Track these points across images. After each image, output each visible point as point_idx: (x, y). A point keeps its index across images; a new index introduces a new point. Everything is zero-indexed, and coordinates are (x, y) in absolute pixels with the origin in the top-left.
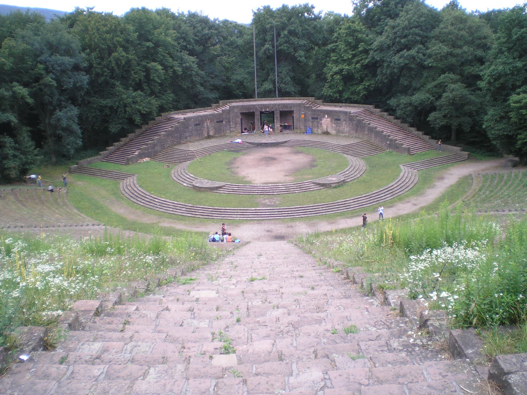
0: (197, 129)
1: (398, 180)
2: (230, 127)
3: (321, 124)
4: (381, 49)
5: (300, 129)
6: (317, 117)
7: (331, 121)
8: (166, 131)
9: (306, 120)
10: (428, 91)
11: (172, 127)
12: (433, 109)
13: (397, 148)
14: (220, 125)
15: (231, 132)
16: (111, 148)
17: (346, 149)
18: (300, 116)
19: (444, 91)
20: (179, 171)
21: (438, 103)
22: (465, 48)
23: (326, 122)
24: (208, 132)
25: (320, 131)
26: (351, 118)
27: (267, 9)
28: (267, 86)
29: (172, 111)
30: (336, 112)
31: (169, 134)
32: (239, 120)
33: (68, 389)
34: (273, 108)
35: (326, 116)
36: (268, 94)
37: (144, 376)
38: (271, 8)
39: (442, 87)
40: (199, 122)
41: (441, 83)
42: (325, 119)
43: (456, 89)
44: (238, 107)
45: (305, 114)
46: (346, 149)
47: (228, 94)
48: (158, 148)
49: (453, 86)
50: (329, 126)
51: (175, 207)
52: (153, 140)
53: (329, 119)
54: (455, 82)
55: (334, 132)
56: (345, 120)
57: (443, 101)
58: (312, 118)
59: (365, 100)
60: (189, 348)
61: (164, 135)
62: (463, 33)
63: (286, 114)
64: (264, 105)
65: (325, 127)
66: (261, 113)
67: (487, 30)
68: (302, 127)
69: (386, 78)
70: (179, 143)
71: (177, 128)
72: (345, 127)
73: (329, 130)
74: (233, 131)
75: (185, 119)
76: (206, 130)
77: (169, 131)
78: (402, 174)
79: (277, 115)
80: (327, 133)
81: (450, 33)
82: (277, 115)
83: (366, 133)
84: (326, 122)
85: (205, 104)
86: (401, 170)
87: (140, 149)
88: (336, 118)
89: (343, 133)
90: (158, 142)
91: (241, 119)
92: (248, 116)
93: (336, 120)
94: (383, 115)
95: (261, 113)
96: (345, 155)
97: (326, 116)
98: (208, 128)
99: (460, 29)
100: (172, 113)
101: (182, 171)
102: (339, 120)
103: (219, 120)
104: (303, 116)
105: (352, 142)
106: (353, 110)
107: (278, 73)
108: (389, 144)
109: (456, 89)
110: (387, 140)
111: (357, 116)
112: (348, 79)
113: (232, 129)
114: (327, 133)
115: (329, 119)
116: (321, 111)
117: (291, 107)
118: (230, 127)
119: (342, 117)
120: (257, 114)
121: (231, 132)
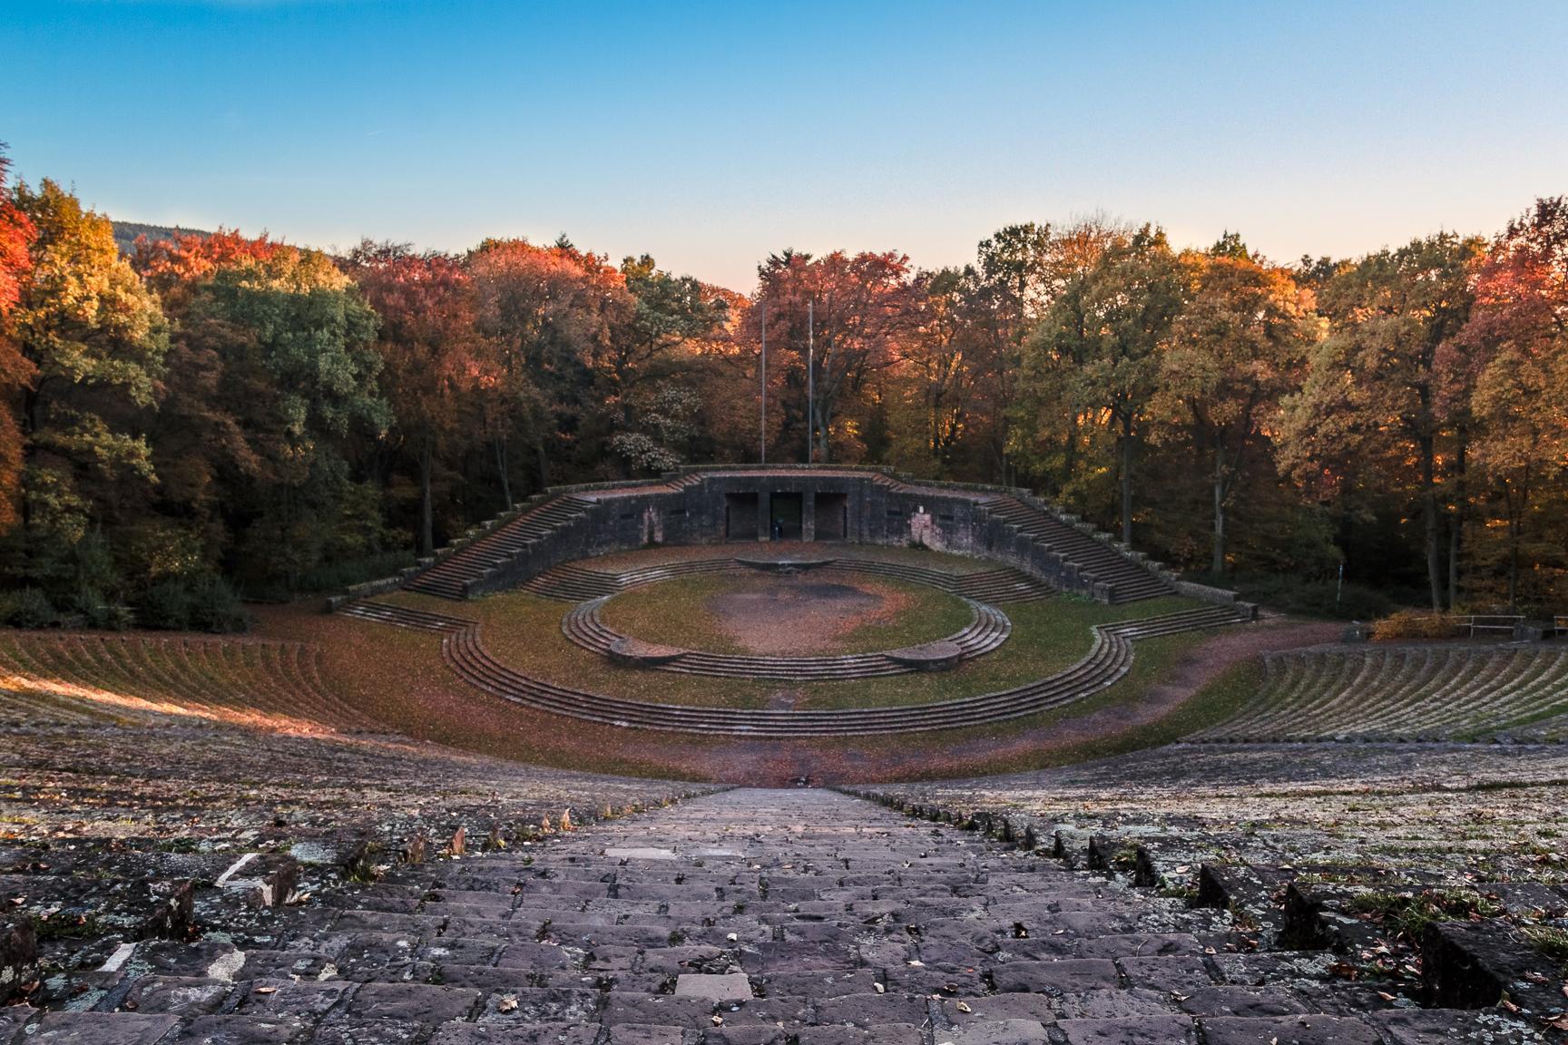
1: (1087, 658)
7: (933, 522)
8: (555, 528)
24: (651, 534)
26: (974, 517)
27: (794, 262)
30: (945, 500)
33: (1190, 971)
37: (221, 1004)
38: (952, 270)
51: (1342, 702)
53: (927, 517)
58: (890, 513)
60: (606, 959)
66: (774, 496)
67: (1299, 303)
71: (579, 521)
73: (926, 541)
78: (1095, 647)
79: (810, 503)
82: (810, 503)
86: (1093, 639)
88: (945, 517)
95: (774, 496)
98: (651, 527)
101: (588, 619)
102: (951, 518)
108: (1066, 578)
115: (927, 517)
119: (958, 512)
120: (765, 497)
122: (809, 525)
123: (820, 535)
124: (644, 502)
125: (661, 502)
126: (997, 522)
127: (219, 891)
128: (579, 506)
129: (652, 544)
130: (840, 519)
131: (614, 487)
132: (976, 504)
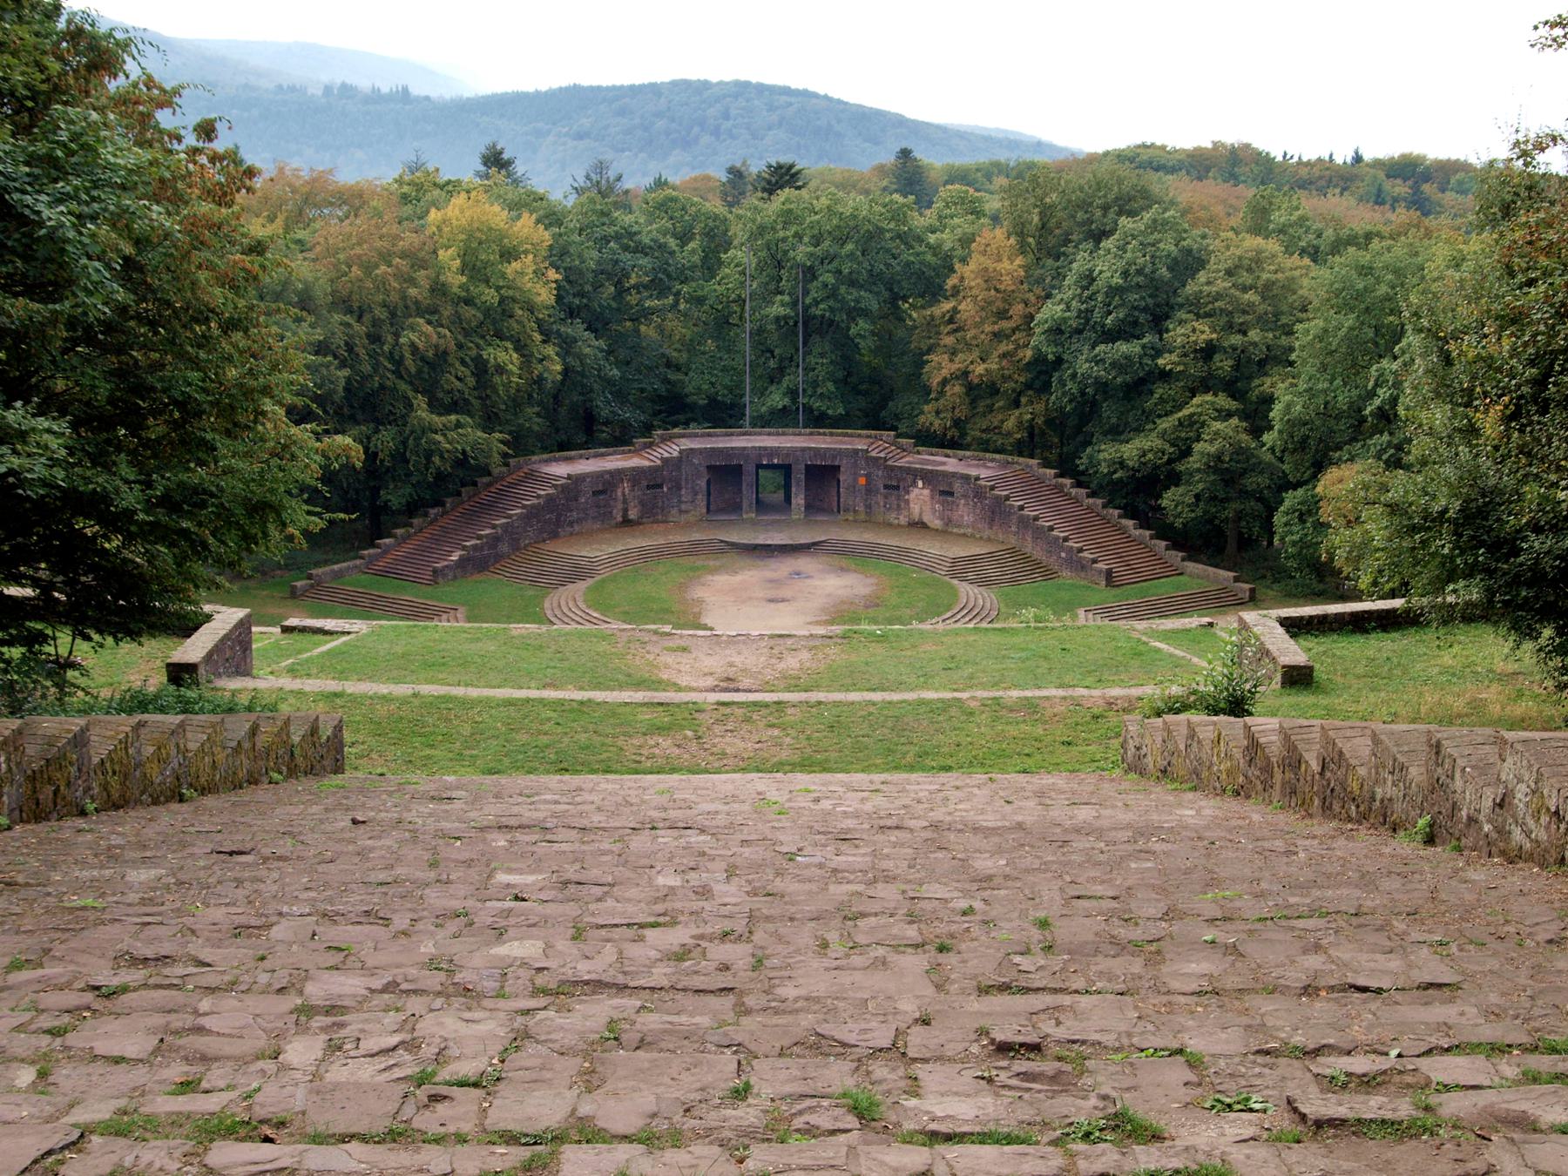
0: (592, 506)
2: (680, 502)
3: (907, 502)
4: (1057, 331)
5: (855, 511)
6: (898, 483)
8: (524, 507)
9: (870, 490)
10: (1163, 435)
11: (539, 497)
12: (1174, 479)
13: (1083, 567)
14: (656, 493)
15: (681, 511)
16: (387, 541)
17: (959, 568)
18: (855, 480)
19: (1198, 439)
20: (563, 603)
21: (1181, 467)
22: (1254, 335)
23: (920, 499)
24: (625, 511)
25: (903, 520)
26: (978, 492)
28: (777, 399)
29: (533, 453)
31: (532, 514)
32: (703, 483)
34: (788, 455)
35: (920, 484)
36: (780, 419)
39: (1194, 426)
40: (606, 484)
41: (1192, 415)
42: (916, 491)
43: (1221, 433)
44: (701, 451)
45: (867, 476)
46: (959, 568)
47: (674, 410)
48: (504, 548)
49: (1217, 425)
50: (927, 508)
52: (494, 527)
53: (926, 492)
54: (1226, 415)
55: (937, 523)
56: (964, 496)
57: (1194, 462)
59: (1028, 445)
61: (520, 516)
62: (1251, 296)
63: (822, 475)
64: (765, 448)
65: (915, 509)
66: (759, 466)
68: (861, 508)
69: (1070, 401)
70: (554, 536)
71: (550, 498)
72: (965, 513)
73: (926, 519)
74: (687, 512)
75: (569, 477)
76: (620, 506)
77: (532, 506)
79: (799, 475)
80: (919, 525)
81: (1218, 296)
82: (799, 475)
83: (1014, 529)
84: (920, 499)
85: (621, 439)
87: (464, 548)
88: (944, 488)
89: (959, 526)
90: (505, 531)
91: (708, 483)
92: (726, 476)
93: (943, 493)
94: (1063, 486)
96: (955, 582)
97: (920, 484)
98: (625, 501)
99: (1245, 289)
100: (534, 458)
101: (571, 604)
102: (951, 494)
103: (652, 482)
104: (862, 481)
105: (978, 551)
106: (983, 470)
107: (805, 354)
109: (1221, 433)
110: (1062, 549)
111: (992, 488)
112: (980, 392)
113: (683, 507)
114: (919, 525)
115: (926, 492)
116: (908, 470)
117: (834, 457)
118: (680, 502)
119: (957, 487)
120: (749, 468)
121: (681, 511)
122: (799, 500)
123: (809, 507)
124: (617, 475)
125: (636, 475)
126: (998, 497)
127: (564, 363)
128: (546, 479)
129: (627, 522)
130: (834, 493)
131: (696, 436)
132: (978, 478)
